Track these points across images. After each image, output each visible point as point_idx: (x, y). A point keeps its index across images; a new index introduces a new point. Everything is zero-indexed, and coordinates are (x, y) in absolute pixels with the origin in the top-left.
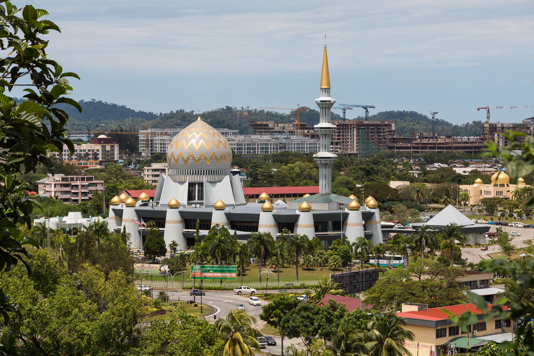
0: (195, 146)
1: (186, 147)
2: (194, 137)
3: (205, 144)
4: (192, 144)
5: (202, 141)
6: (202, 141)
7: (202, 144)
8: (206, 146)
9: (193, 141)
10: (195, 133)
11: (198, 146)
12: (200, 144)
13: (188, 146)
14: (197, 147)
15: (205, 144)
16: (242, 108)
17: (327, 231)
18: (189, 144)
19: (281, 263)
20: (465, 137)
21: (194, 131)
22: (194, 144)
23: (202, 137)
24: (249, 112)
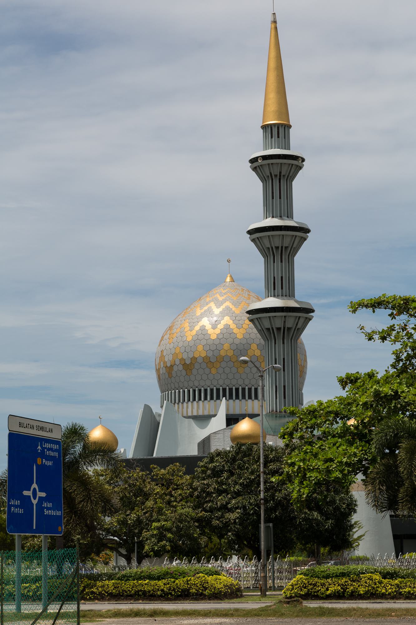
0: (210, 331)
1: (189, 336)
2: (209, 312)
3: (233, 326)
4: (203, 328)
5: (227, 320)
6: (227, 320)
7: (227, 327)
8: (236, 331)
9: (205, 322)
10: (212, 305)
11: (218, 331)
12: (220, 326)
13: (194, 332)
14: (214, 334)
15: (233, 326)
16: (374, 312)
17: (265, 522)
18: (197, 328)
19: (315, 432)
20: (52, 611)
21: (210, 302)
22: (208, 327)
23: (227, 312)
24: (12, 621)
